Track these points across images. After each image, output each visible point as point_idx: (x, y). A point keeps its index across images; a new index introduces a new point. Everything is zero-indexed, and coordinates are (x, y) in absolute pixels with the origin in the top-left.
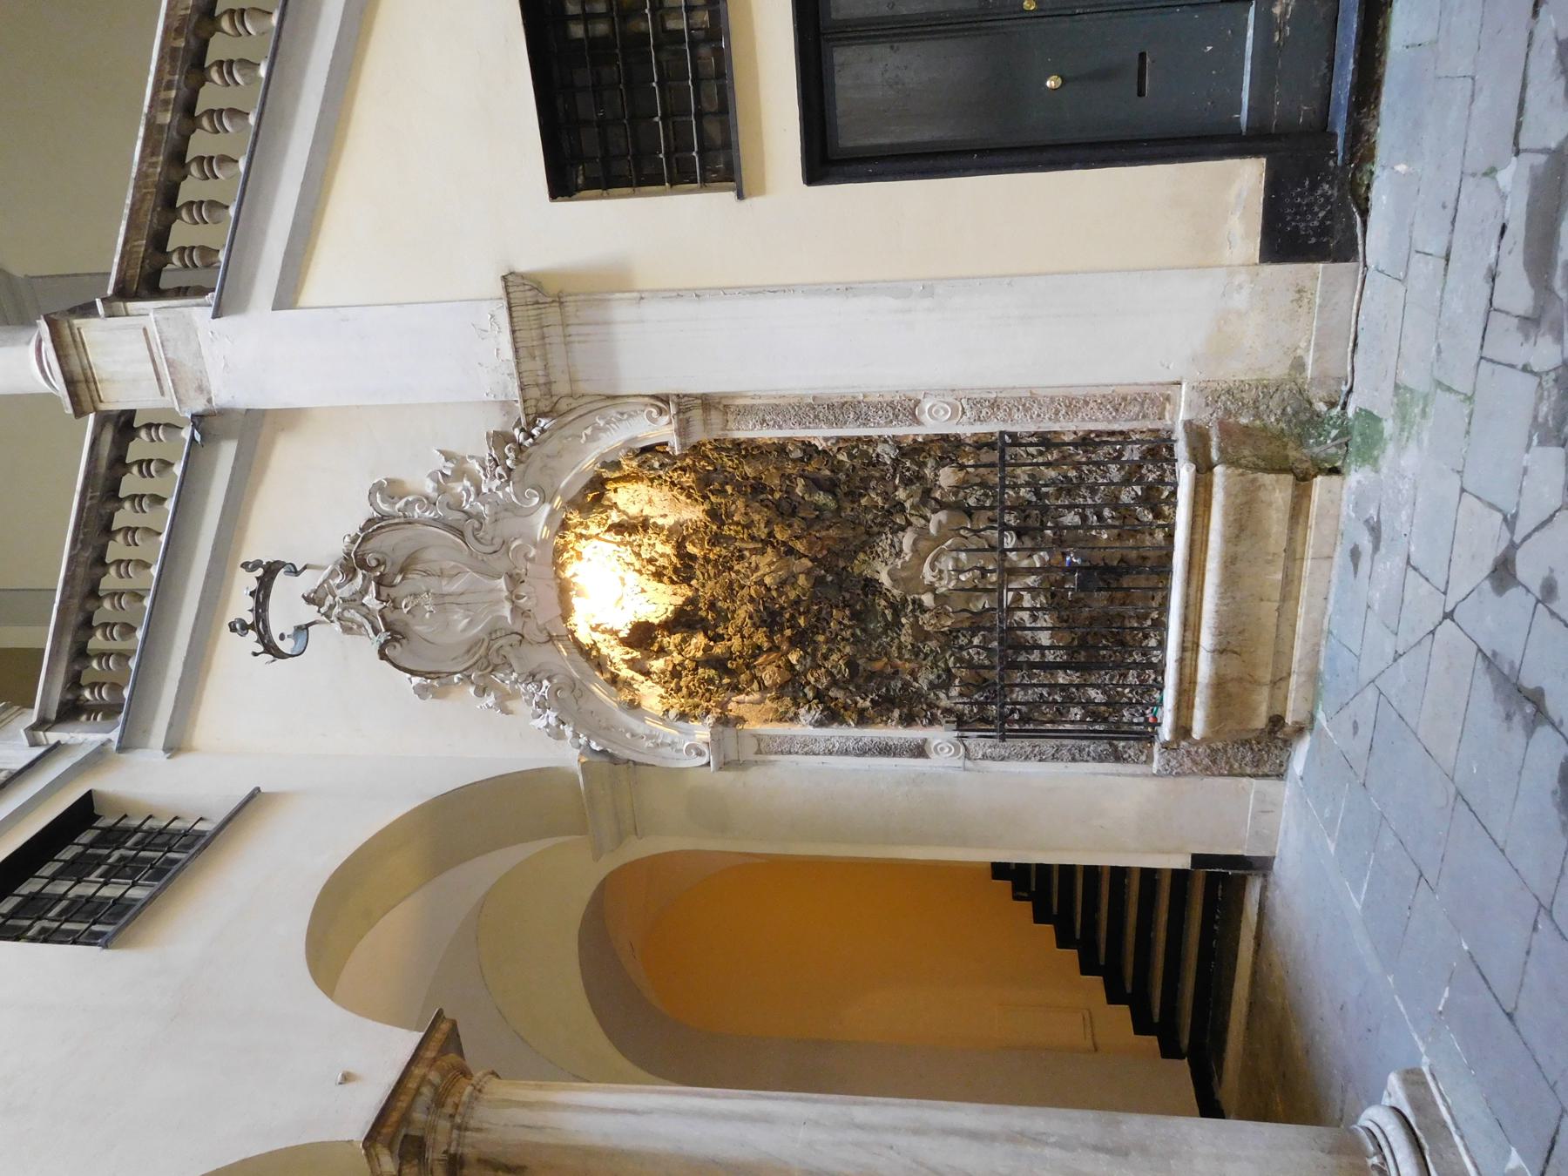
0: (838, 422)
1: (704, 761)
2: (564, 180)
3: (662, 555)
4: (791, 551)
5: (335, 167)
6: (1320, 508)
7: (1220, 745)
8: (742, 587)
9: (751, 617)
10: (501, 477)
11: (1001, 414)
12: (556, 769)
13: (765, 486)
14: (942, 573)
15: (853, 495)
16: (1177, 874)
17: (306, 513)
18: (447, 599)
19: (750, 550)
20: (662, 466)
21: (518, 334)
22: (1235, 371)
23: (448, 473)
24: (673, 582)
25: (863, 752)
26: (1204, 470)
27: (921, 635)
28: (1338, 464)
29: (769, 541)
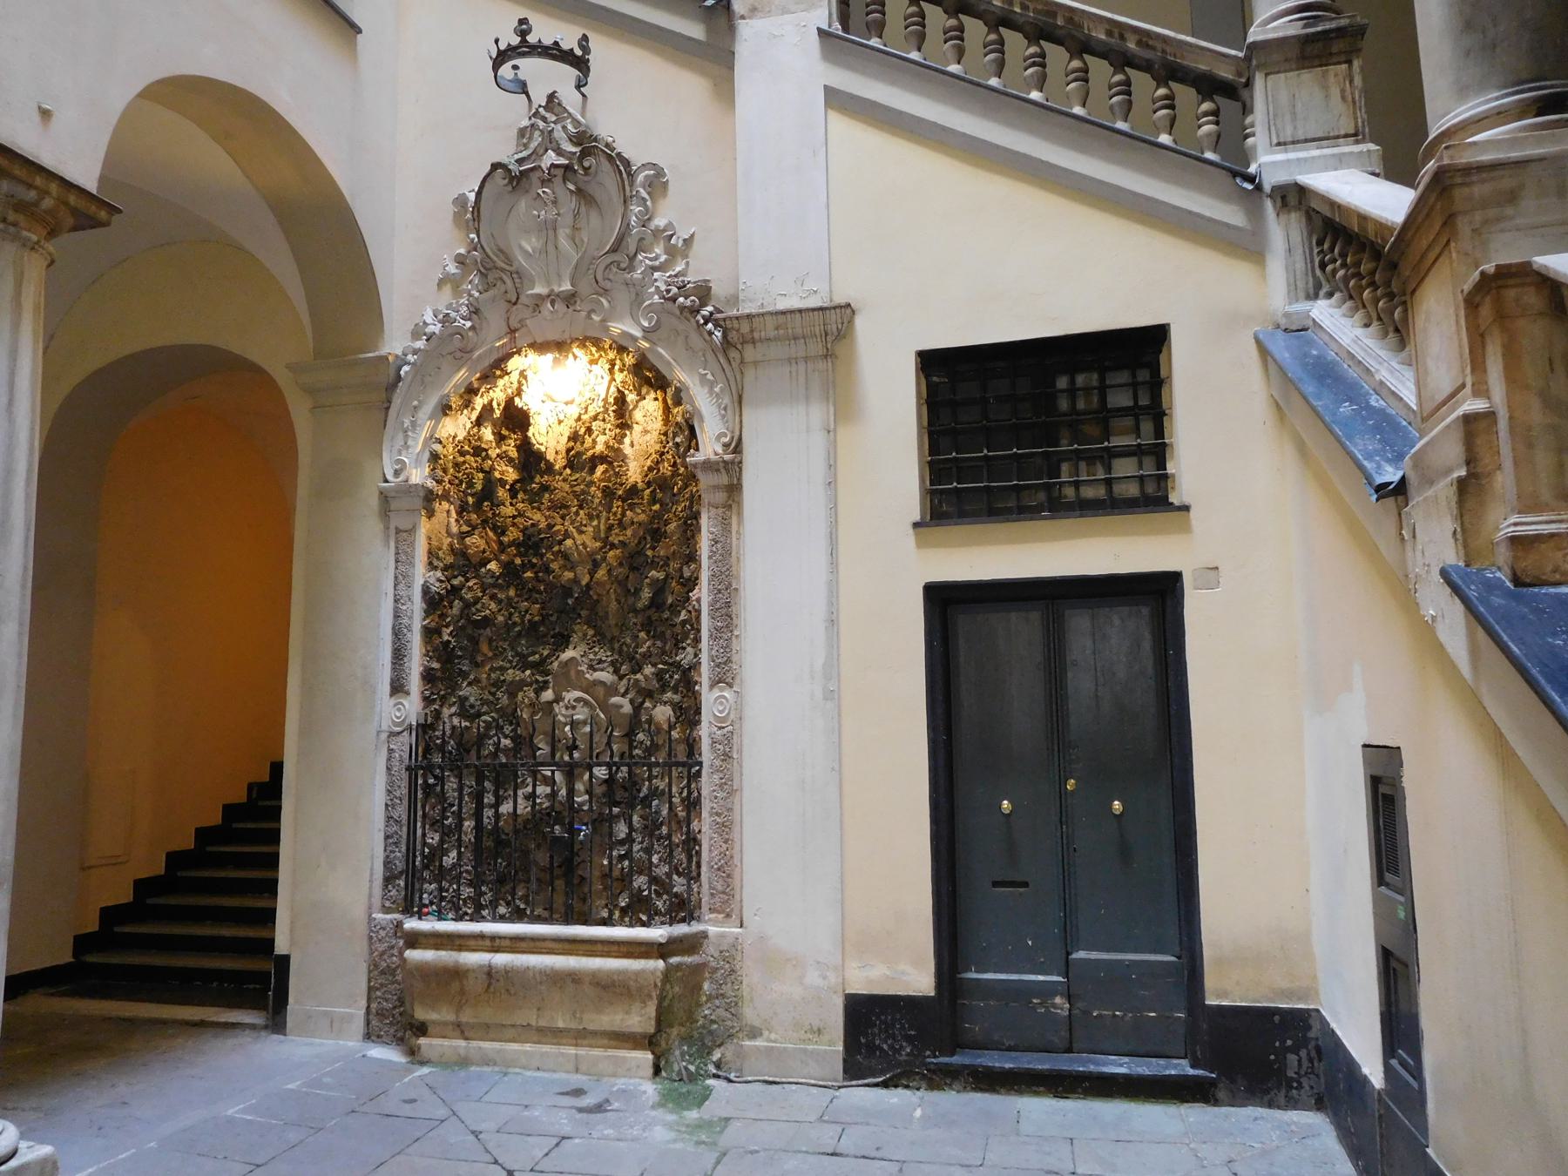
1: (390, 477)
3: (594, 442)
4: (596, 565)
7: (399, 978)
8: (563, 517)
11: (718, 763)
14: (572, 708)
15: (648, 626)
18: (551, 233)
22: (751, 976)
24: (568, 451)
25: (397, 633)
27: (514, 689)
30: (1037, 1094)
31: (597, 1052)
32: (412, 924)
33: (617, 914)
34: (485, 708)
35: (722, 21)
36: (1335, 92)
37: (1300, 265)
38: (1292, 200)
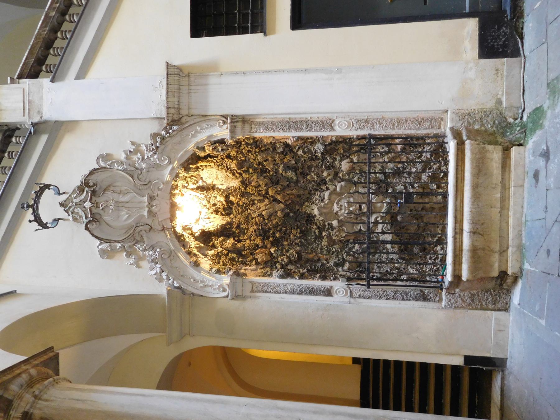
0: (299, 129)
1: (225, 294)
2: (197, 30)
3: (219, 201)
4: (275, 200)
6: (515, 161)
7: (475, 292)
8: (252, 218)
9: (255, 231)
10: (153, 149)
11: (369, 126)
12: (156, 295)
13: (266, 169)
14: (342, 208)
15: (304, 175)
16: (455, 369)
17: (67, 168)
18: (120, 204)
19: (258, 200)
20: (222, 150)
21: (169, 86)
22: (471, 105)
23: (132, 150)
24: (222, 214)
25: (302, 292)
26: (460, 145)
28: (522, 142)
31: (512, 175)
32: (449, 278)
33: (440, 190)
34: (340, 256)
35: (42, 126)
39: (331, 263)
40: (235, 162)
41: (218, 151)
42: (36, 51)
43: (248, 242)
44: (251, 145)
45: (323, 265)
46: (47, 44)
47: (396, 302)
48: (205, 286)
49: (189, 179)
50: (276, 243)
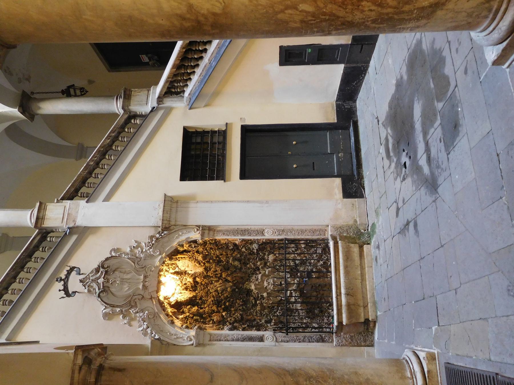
1: (191, 343)
2: (184, 176)
4: (227, 280)
5: (130, 172)
7: (353, 334)
8: (211, 293)
9: (212, 301)
11: (285, 233)
14: (269, 284)
15: (245, 264)
17: (88, 257)
18: (124, 280)
20: (195, 247)
22: (341, 222)
24: (190, 291)
25: (244, 339)
27: (263, 308)
29: (220, 278)
30: (361, 155)
32: (336, 323)
34: (269, 317)
36: (139, 93)
37: (175, 99)
38: (161, 100)
39: (263, 321)
40: (201, 255)
41: (192, 247)
42: (76, 184)
43: (207, 308)
44: (213, 244)
45: (258, 323)
46: (83, 181)
47: (305, 344)
48: (177, 338)
49: (170, 266)
50: (225, 309)
